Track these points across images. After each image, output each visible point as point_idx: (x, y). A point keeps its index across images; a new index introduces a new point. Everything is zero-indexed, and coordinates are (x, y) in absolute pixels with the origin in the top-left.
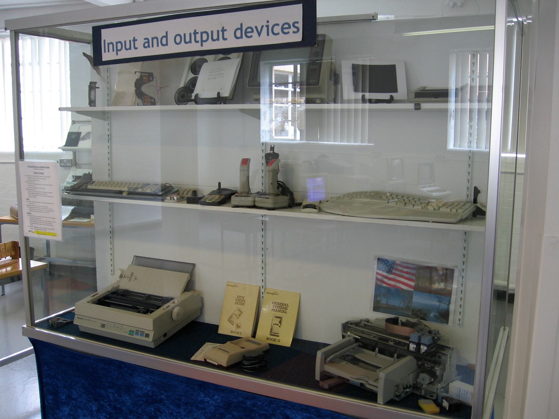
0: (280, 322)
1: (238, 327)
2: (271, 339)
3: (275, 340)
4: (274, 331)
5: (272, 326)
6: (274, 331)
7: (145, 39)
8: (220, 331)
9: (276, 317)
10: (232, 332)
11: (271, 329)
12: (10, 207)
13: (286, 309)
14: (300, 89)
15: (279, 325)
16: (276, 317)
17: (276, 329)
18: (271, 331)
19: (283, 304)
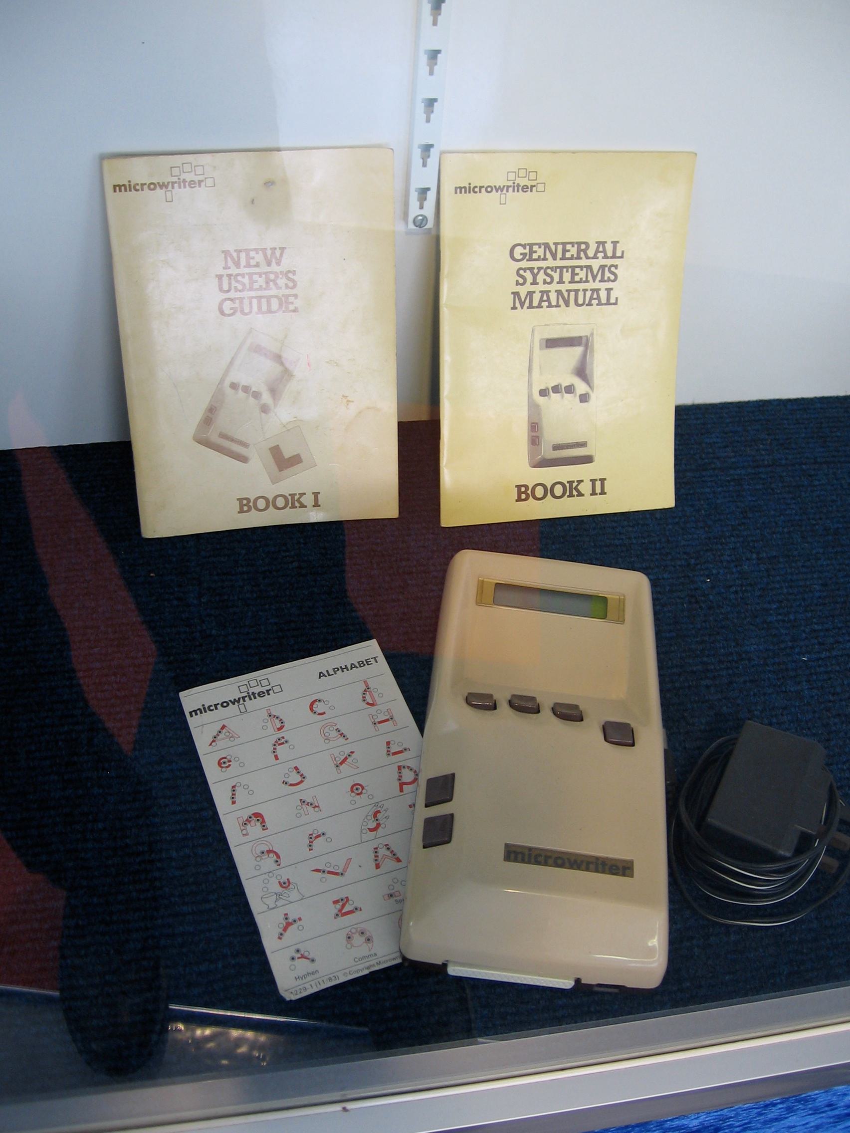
0: (582, 372)
1: (284, 462)
2: (549, 491)
3: (571, 489)
4: (552, 434)
5: (534, 408)
6: (552, 434)
7: (115, 191)
8: (187, 493)
9: (552, 343)
10: (245, 505)
11: (535, 427)
12: (593, 454)
13: (608, 273)
14: (225, 1059)
15: (581, 387)
16: (552, 343)
17: (565, 419)
18: (535, 440)
19: (582, 248)
